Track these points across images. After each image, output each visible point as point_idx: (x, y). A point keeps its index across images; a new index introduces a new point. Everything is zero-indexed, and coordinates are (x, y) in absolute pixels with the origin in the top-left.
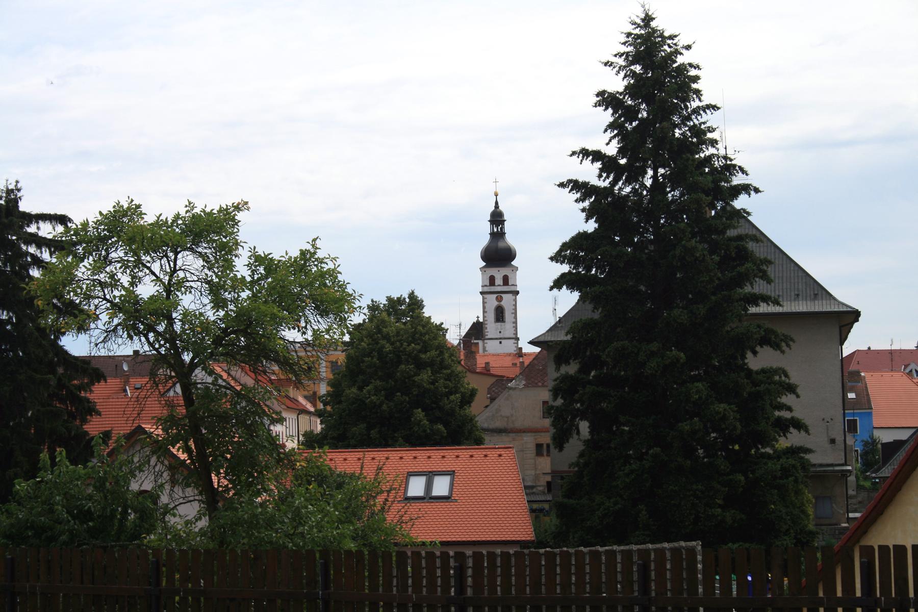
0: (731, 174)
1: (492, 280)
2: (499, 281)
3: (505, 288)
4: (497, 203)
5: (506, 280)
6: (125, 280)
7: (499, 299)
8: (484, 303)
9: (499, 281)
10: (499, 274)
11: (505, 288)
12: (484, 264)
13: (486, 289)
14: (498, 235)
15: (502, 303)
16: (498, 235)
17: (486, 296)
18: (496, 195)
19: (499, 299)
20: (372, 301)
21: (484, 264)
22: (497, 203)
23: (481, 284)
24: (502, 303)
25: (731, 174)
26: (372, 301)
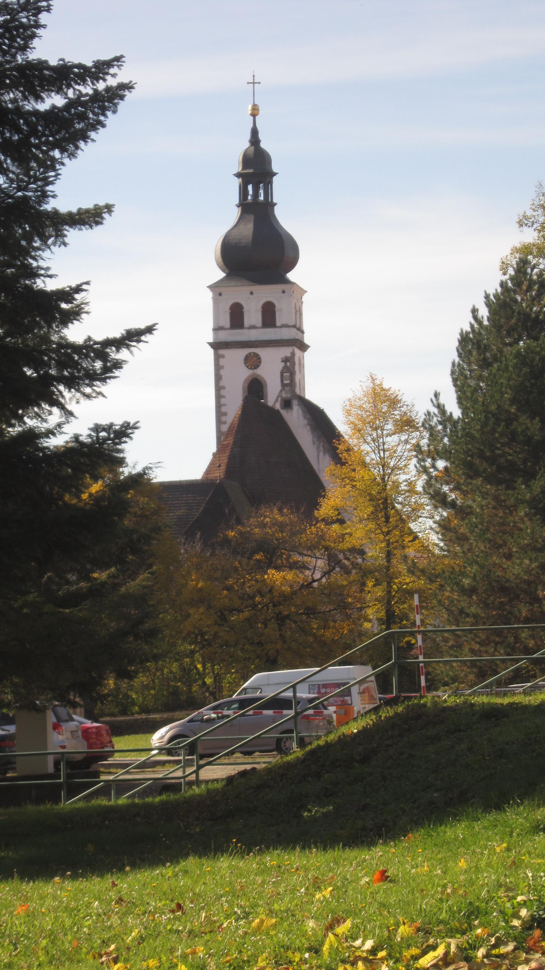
0: (411, 829)
1: (237, 315)
2: (253, 315)
3: (270, 334)
4: (255, 132)
5: (269, 314)
6: (463, 901)
7: (253, 362)
8: (218, 368)
9: (253, 315)
10: (253, 298)
11: (270, 334)
12: (222, 275)
13: (225, 336)
14: (257, 209)
15: (261, 372)
16: (257, 209)
17: (221, 352)
18: (254, 114)
19: (253, 362)
20: (65, 244)
21: (222, 275)
22: (255, 132)
23: (210, 324)
24: (261, 372)
25: (411, 829)
26: (65, 244)
